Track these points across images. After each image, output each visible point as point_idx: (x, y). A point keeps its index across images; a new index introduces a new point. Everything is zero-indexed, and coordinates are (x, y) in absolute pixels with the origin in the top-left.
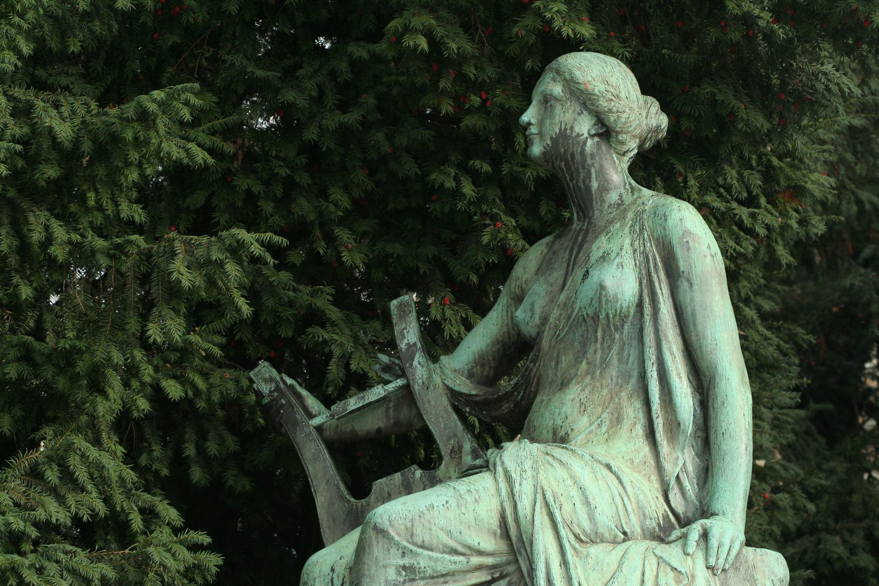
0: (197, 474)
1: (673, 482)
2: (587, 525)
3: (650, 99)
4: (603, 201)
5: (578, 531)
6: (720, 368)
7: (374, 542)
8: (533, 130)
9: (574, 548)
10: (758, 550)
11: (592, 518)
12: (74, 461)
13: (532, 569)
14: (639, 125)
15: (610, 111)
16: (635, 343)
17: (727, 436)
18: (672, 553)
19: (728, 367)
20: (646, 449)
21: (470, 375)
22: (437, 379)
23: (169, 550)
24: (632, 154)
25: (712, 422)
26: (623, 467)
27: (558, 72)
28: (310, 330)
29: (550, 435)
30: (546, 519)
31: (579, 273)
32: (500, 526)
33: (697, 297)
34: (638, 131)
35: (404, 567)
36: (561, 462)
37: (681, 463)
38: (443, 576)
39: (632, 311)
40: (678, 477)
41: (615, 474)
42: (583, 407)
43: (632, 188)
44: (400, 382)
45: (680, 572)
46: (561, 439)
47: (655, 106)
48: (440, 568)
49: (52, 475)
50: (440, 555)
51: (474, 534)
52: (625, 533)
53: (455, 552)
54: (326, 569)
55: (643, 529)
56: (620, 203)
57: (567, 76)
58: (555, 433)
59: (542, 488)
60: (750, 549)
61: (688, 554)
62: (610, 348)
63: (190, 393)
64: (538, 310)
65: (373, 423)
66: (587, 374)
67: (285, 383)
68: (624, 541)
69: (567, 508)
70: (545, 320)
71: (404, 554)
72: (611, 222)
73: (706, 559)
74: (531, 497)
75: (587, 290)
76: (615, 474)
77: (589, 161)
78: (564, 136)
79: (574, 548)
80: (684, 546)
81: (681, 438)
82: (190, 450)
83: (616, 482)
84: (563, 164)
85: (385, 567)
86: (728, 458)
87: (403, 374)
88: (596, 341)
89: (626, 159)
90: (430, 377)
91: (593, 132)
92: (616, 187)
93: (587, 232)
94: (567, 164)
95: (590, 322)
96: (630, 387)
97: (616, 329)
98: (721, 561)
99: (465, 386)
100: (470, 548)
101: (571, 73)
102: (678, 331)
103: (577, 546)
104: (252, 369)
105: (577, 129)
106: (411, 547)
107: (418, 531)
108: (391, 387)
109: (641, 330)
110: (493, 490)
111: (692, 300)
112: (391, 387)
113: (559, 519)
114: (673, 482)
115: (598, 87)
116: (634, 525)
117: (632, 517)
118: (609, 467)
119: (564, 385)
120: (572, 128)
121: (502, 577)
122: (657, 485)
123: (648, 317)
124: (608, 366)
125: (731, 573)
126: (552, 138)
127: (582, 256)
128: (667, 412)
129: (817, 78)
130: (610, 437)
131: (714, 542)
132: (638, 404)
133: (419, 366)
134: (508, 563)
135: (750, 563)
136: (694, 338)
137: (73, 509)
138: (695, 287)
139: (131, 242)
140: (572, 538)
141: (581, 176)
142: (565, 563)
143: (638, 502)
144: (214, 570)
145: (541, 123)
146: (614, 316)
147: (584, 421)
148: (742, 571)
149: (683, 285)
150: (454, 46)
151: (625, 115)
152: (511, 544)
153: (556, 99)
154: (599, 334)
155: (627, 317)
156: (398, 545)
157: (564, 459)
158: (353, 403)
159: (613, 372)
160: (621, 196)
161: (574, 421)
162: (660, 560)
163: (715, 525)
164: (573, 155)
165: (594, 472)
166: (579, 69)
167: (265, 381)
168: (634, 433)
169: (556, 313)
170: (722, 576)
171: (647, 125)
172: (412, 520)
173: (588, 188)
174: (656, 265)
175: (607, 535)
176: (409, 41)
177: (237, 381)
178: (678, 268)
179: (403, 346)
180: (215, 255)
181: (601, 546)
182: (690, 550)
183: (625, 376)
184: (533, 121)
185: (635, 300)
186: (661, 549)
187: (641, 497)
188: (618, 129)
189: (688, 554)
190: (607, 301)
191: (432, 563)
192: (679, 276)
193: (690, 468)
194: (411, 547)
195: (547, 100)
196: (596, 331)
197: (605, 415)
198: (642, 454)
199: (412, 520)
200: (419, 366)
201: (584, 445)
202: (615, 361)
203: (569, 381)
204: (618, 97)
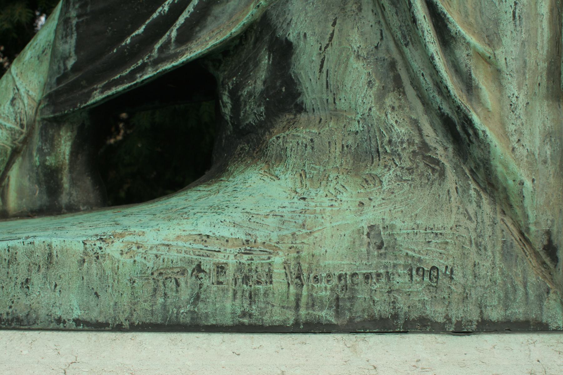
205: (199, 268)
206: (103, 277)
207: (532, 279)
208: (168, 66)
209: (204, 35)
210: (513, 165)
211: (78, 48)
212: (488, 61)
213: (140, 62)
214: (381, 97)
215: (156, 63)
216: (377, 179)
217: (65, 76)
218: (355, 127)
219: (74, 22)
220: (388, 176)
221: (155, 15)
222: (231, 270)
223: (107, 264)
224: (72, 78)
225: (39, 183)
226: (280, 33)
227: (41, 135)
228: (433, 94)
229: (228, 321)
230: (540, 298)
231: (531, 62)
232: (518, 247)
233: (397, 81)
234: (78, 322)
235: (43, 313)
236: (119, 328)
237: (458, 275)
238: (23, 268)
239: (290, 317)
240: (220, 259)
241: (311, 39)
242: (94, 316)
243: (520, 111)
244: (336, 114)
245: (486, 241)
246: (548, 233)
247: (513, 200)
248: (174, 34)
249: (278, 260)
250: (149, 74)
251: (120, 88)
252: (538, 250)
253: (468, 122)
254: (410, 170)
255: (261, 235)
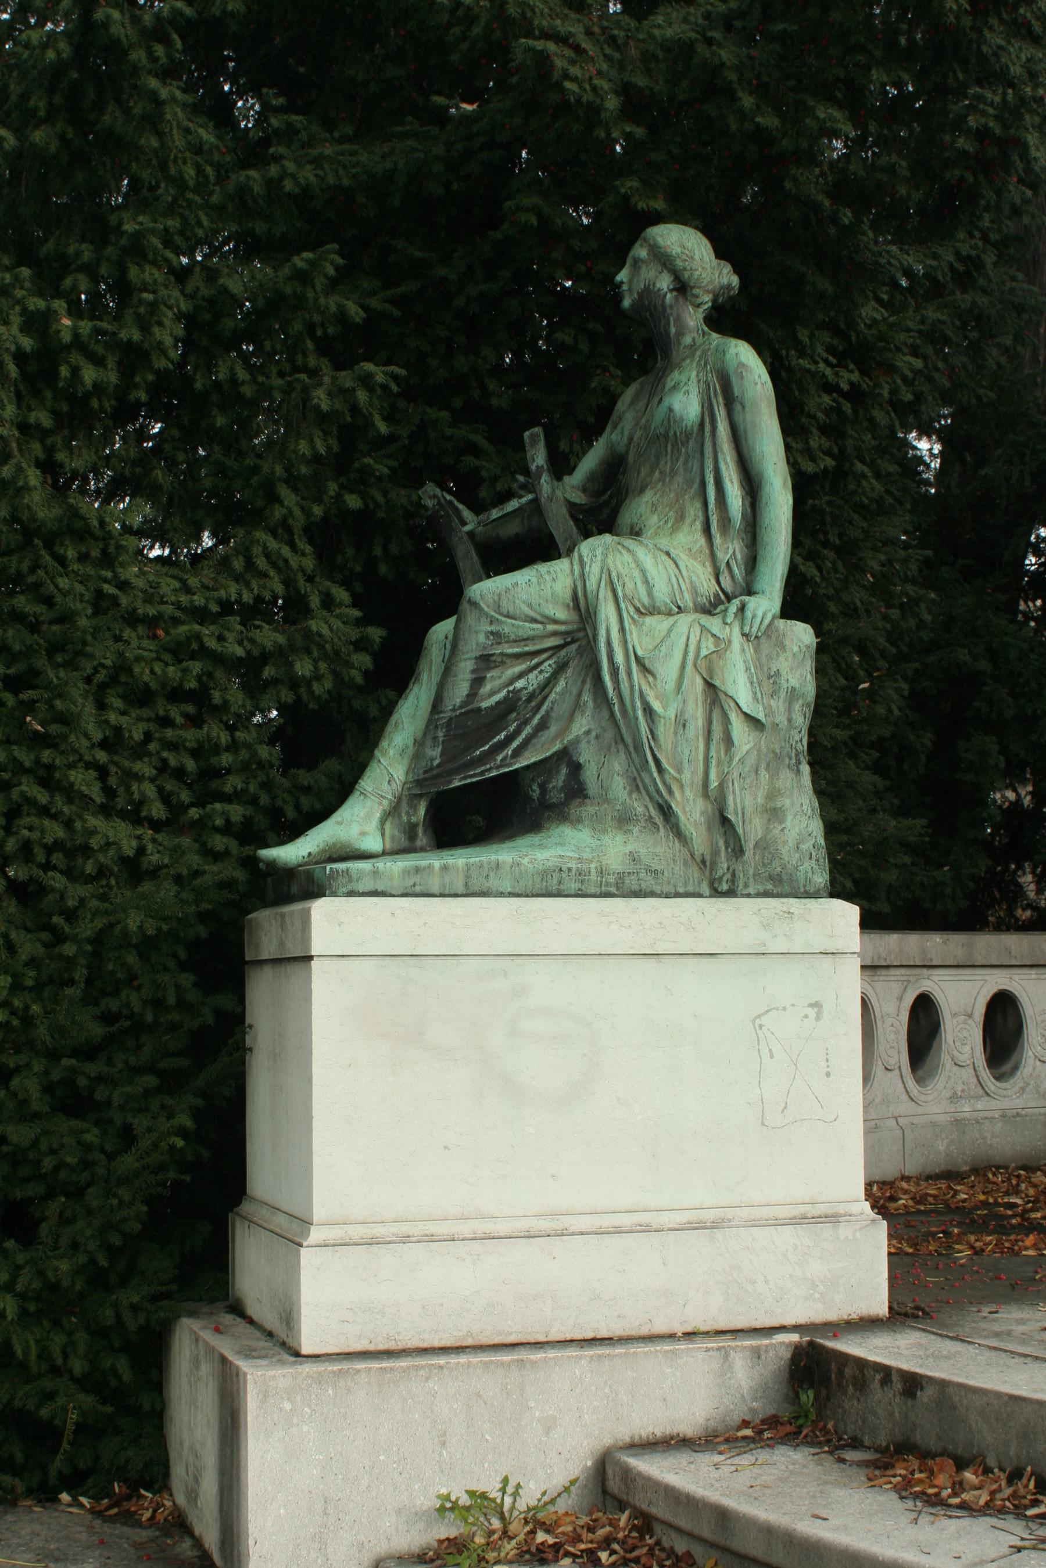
0: (383, 569)
1: (723, 567)
2: (646, 600)
3: (723, 262)
4: (679, 344)
5: (638, 605)
6: (766, 475)
7: (468, 612)
8: (625, 287)
9: (633, 618)
10: (789, 621)
11: (650, 594)
12: (256, 550)
13: (595, 636)
14: (711, 282)
15: (685, 269)
16: (698, 455)
17: (768, 530)
18: (714, 624)
19: (772, 474)
20: (702, 541)
21: (584, 490)
22: (559, 494)
23: (327, 623)
24: (706, 307)
25: (758, 518)
26: (682, 555)
27: (645, 240)
28: (463, 458)
29: (629, 530)
30: (610, 594)
31: (656, 399)
32: (573, 600)
33: (749, 417)
34: (710, 287)
35: (492, 633)
36: (629, 550)
37: (731, 551)
38: (525, 640)
39: (695, 430)
40: (728, 563)
41: (673, 559)
42: (654, 508)
43: (704, 333)
44: (530, 497)
45: (719, 638)
46: (636, 533)
47: (727, 268)
48: (521, 633)
49: (238, 564)
50: (521, 623)
51: (551, 606)
52: (679, 607)
53: (534, 621)
54: (441, 637)
55: (695, 604)
56: (693, 346)
57: (651, 242)
58: (632, 528)
59: (609, 570)
60: (782, 621)
61: (726, 624)
62: (677, 460)
63: (371, 505)
64: (626, 433)
65: (513, 528)
66: (659, 481)
67: (445, 498)
68: (678, 613)
69: (630, 585)
70: (631, 439)
71: (491, 623)
72: (683, 360)
73: (742, 628)
74: (597, 576)
75: (660, 414)
76: (673, 559)
77: (668, 311)
78: (648, 292)
79: (633, 618)
80: (724, 618)
81: (732, 531)
82: (378, 551)
83: (673, 566)
84: (648, 314)
85: (476, 632)
86: (769, 548)
87: (534, 492)
88: (666, 454)
89: (701, 310)
90: (553, 492)
91: (671, 287)
92: (690, 332)
93: (665, 369)
94: (651, 314)
95: (662, 439)
96: (693, 491)
97: (683, 444)
98: (755, 629)
99: (578, 498)
100: (547, 617)
101: (654, 239)
102: (733, 445)
103: (636, 616)
104: (418, 489)
105: (658, 285)
106: (497, 616)
107: (504, 603)
108: (524, 500)
109: (703, 445)
110: (568, 571)
111: (744, 420)
112: (524, 500)
113: (620, 594)
114: (723, 567)
115: (676, 250)
116: (687, 600)
117: (686, 594)
118: (668, 554)
119: (642, 491)
120: (654, 284)
121: (573, 641)
122: (710, 569)
123: (707, 434)
124: (676, 474)
125: (763, 640)
126: (638, 293)
127: (659, 387)
128: (721, 510)
129: (881, 255)
130: (674, 530)
131: (749, 614)
132: (698, 505)
133: (545, 482)
134: (579, 630)
135: (781, 632)
136: (745, 451)
137: (256, 592)
138: (747, 409)
139: (297, 380)
140: (632, 610)
141: (663, 322)
142: (622, 629)
143: (691, 582)
144: (378, 640)
145: (630, 281)
146: (681, 433)
147: (654, 519)
148: (773, 638)
149: (738, 407)
150: (559, 222)
151: (698, 273)
152: (581, 616)
153: (642, 261)
154: (669, 449)
155: (691, 434)
156: (487, 615)
157: (631, 548)
158: (495, 513)
159: (680, 479)
160: (694, 339)
161: (646, 519)
162: (703, 628)
163: (752, 602)
164: (655, 306)
165: (655, 558)
166: (661, 236)
167: (430, 497)
168: (694, 528)
169: (639, 433)
170: (755, 642)
171: (719, 283)
172: (499, 595)
173: (668, 333)
174: (715, 391)
175: (663, 608)
176: (522, 218)
177: (409, 497)
178: (733, 394)
179: (533, 468)
180: (348, 384)
181: (656, 617)
182: (729, 621)
183: (689, 483)
184: (625, 280)
185: (697, 420)
186: (705, 620)
187: (694, 578)
188: (692, 284)
189: (726, 624)
190: (675, 421)
191: (515, 630)
192: (734, 401)
193: (739, 556)
194: (497, 616)
195: (636, 262)
196: (666, 447)
197: (671, 513)
198: (698, 545)
199: (499, 595)
200: (545, 482)
201: (652, 538)
202: (681, 471)
203: (646, 487)
204: (692, 258)
205: (561, 870)
206: (521, 873)
207: (696, 875)
208: (507, 770)
209: (527, 754)
210: (688, 826)
211: (442, 754)
212: (679, 781)
213: (488, 766)
214: (630, 794)
215: (498, 767)
216: (631, 831)
217: (431, 769)
218: (618, 807)
219: (441, 739)
220: (636, 830)
221: (495, 740)
222: (574, 871)
223: (522, 868)
224: (435, 772)
225: (405, 833)
226: (575, 758)
227: (408, 804)
228: (655, 794)
229: (573, 892)
230: (699, 883)
231: (695, 781)
232: (690, 861)
233: (637, 787)
234: (509, 893)
235: (494, 890)
236: (527, 896)
237: (666, 873)
238: (486, 869)
239: (598, 890)
240: (569, 865)
241: (593, 764)
242: (517, 891)
243: (691, 802)
244: (607, 801)
245: (677, 858)
246: (703, 855)
247: (688, 841)
248: (510, 752)
249: (593, 866)
250: (494, 773)
251: (474, 780)
252: (800, 171)
253: (671, 807)
254: (645, 828)
255: (585, 856)
